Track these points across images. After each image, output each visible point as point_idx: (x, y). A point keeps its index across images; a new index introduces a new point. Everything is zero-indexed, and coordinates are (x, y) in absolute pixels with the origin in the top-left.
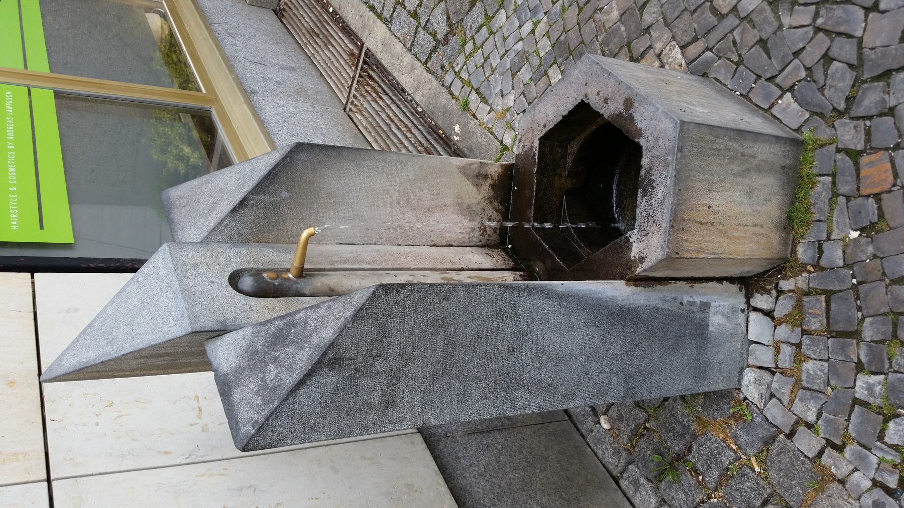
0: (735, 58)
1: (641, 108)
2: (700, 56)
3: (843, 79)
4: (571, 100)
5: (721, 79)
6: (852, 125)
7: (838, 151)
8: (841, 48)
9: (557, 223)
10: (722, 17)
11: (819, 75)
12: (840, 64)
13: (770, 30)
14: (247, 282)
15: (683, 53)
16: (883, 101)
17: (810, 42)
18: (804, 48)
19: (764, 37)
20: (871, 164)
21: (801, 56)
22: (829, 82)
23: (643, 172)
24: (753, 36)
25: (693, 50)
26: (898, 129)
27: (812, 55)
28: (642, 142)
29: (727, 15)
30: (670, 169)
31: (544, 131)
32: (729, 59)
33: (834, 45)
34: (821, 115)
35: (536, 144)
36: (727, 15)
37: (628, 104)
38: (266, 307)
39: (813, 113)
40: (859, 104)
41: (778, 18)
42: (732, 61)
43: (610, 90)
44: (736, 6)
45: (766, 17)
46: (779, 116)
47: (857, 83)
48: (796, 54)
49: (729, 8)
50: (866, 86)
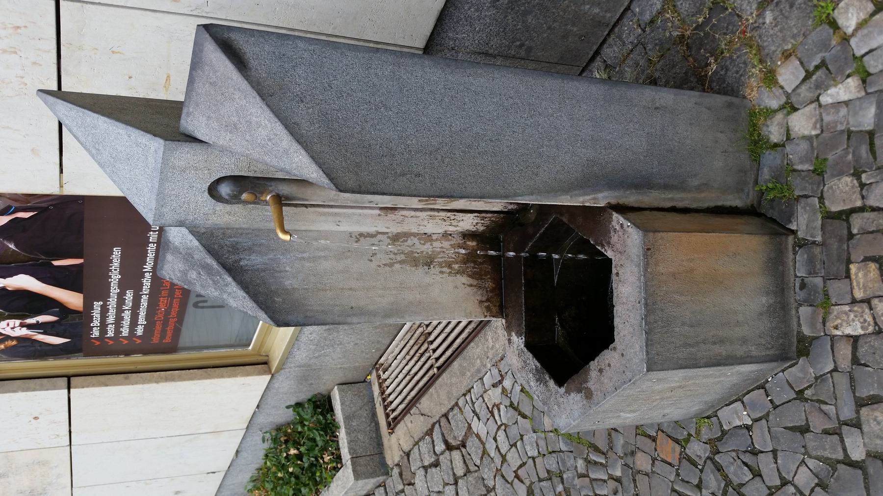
0: (808, 393)
1: (580, 405)
2: (834, 356)
3: (735, 474)
4: (620, 326)
5: (793, 369)
6: (703, 456)
7: (690, 435)
8: (757, 489)
9: (549, 258)
10: (860, 404)
11: (747, 458)
12: (747, 480)
13: (811, 445)
14: (225, 190)
15: (849, 336)
16: (707, 488)
17: (778, 470)
18: (776, 463)
19: (807, 435)
20: (674, 450)
21: (771, 455)
22: (739, 462)
23: (547, 377)
24: (818, 423)
25: (845, 351)
26: (688, 482)
27: (765, 464)
28: (562, 390)
29: (858, 412)
30: (541, 404)
31: (614, 271)
32: (810, 386)
33: (763, 486)
34: (719, 439)
35: (609, 254)
36: (858, 412)
37: (589, 395)
38: (229, 213)
39: (724, 433)
40: (712, 472)
41: (818, 458)
42: (806, 388)
43: (606, 381)
44: (861, 429)
45: (825, 450)
46: (732, 406)
47: (729, 483)
48: (774, 452)
49: (863, 418)
50: (723, 485)
